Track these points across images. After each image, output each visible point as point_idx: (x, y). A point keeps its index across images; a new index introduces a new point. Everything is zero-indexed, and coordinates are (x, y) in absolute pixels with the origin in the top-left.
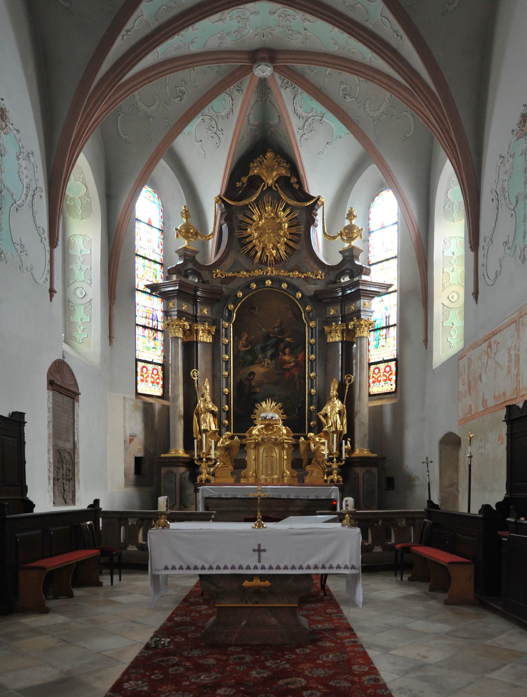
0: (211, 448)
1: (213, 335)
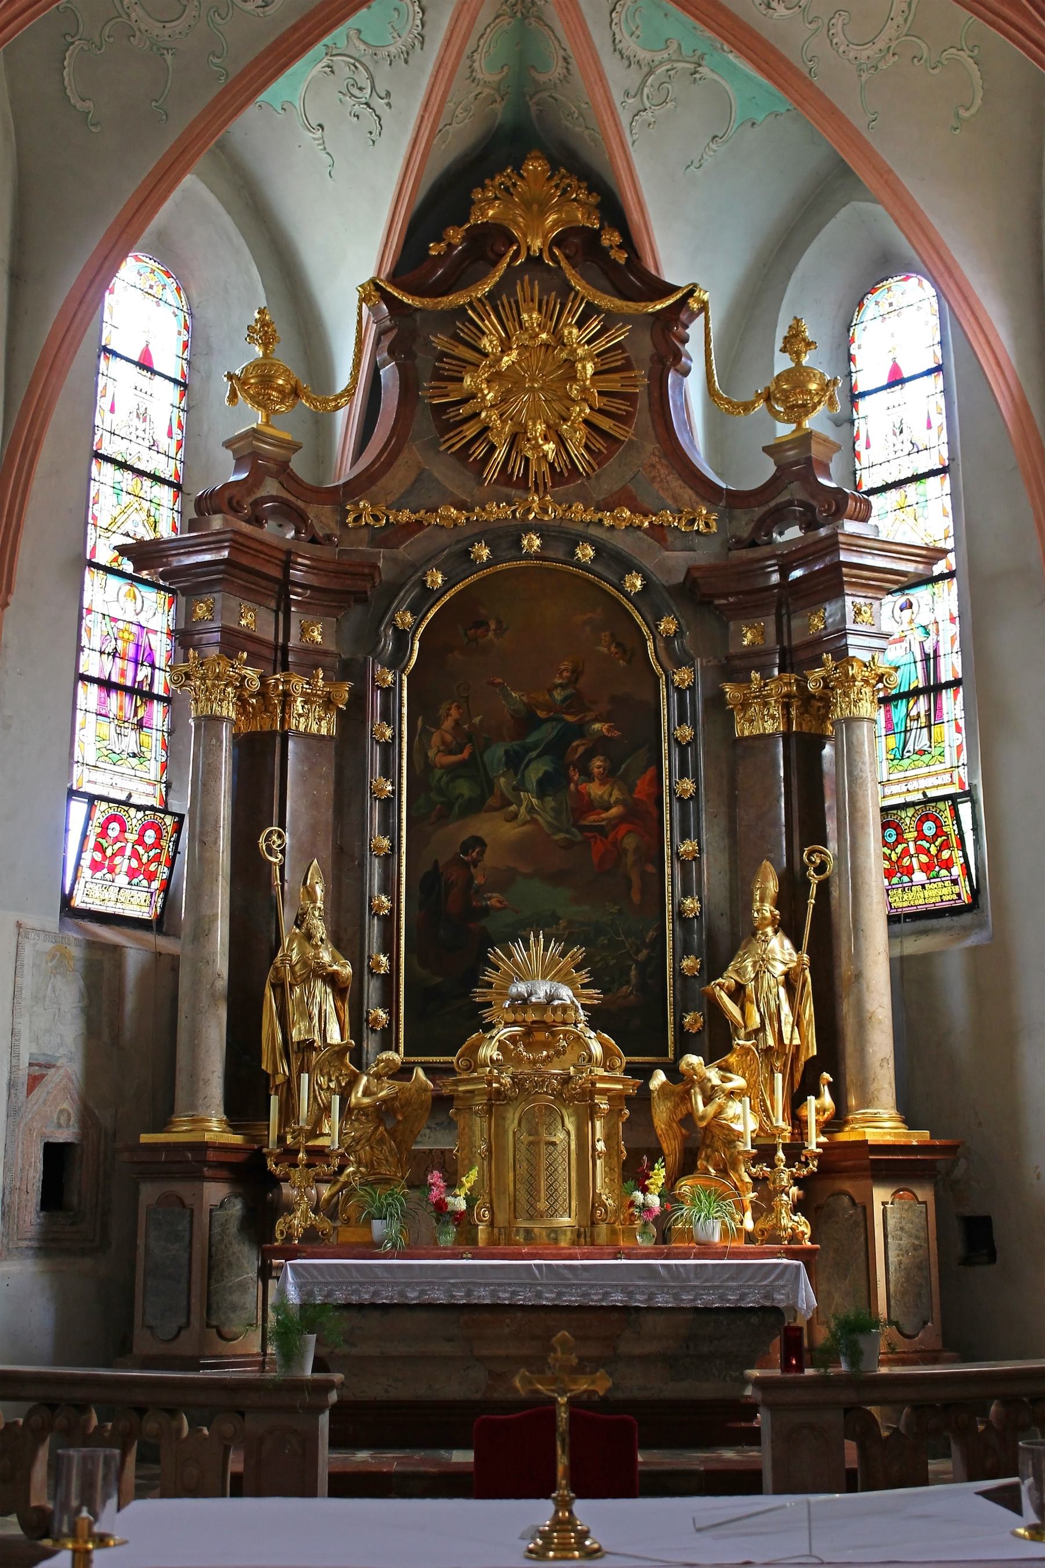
0: (323, 1113)
1: (339, 710)
